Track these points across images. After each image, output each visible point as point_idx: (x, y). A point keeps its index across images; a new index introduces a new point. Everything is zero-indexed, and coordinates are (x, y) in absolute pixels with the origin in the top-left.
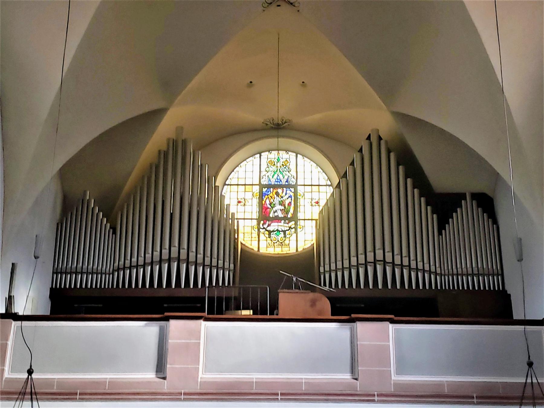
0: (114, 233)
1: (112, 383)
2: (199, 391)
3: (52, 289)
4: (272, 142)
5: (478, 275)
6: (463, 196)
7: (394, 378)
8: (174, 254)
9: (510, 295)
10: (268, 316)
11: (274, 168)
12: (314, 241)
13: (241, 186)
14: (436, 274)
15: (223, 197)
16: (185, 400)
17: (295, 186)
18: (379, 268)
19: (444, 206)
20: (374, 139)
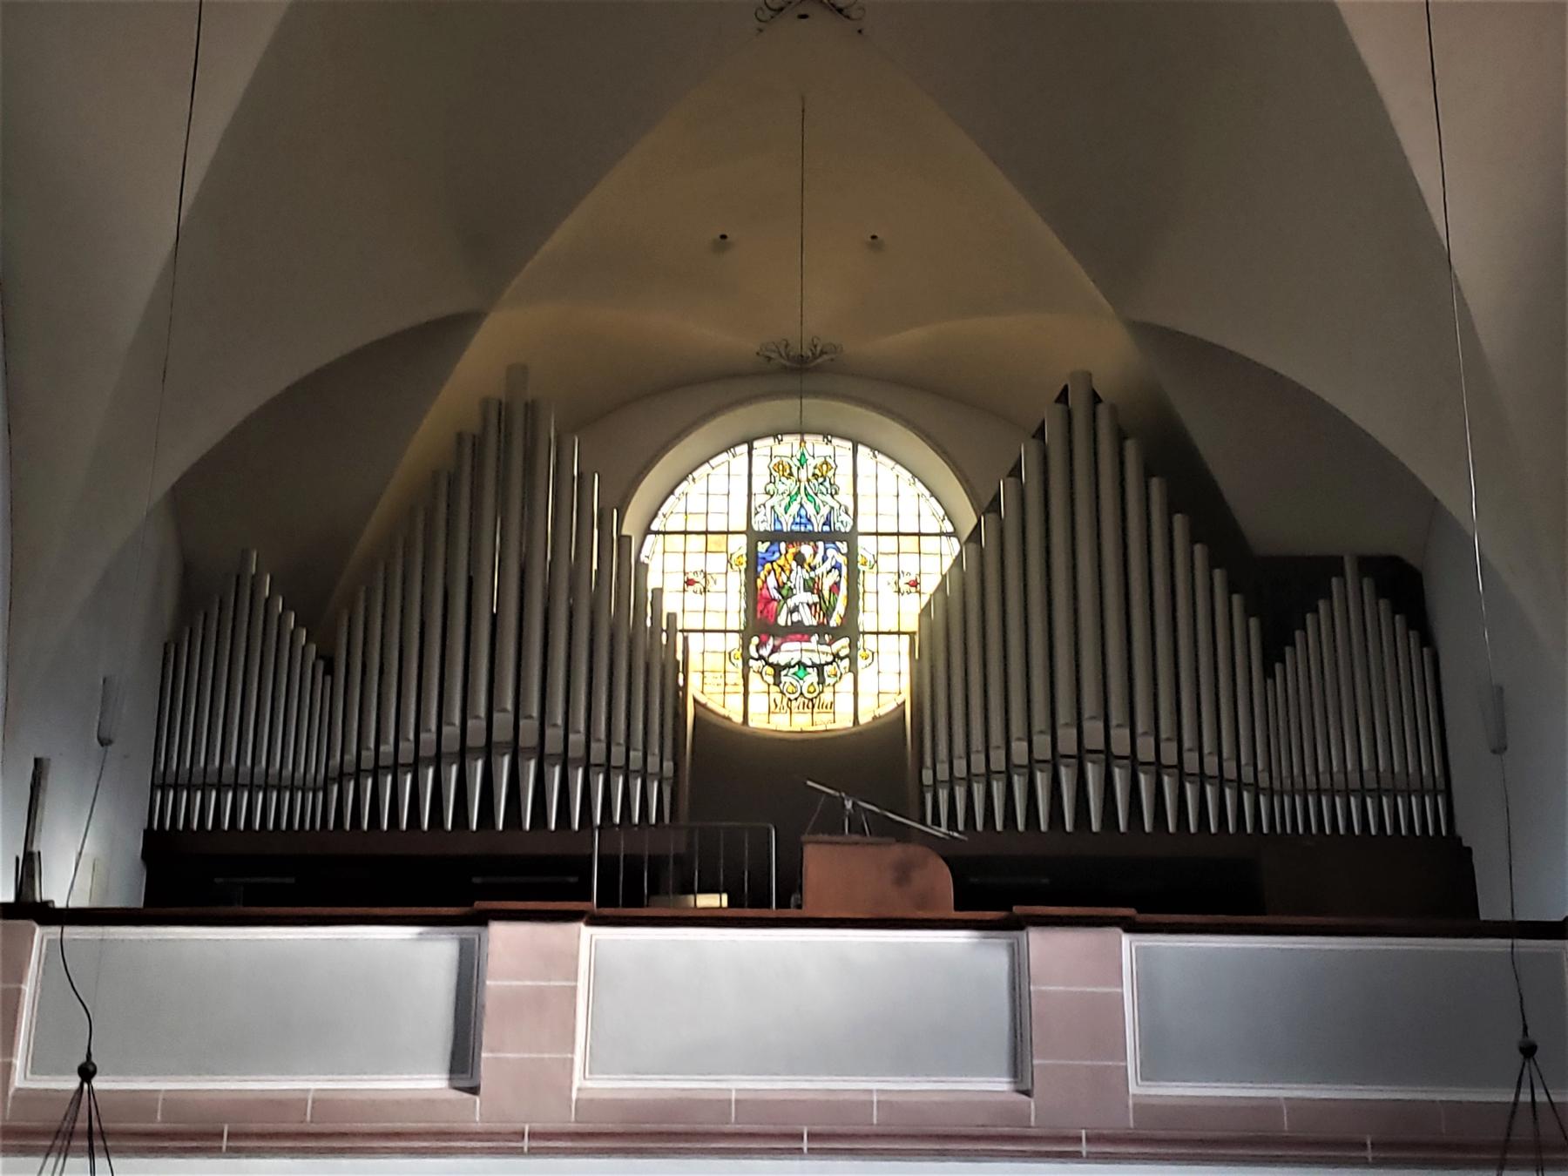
0: (330, 670)
1: (324, 1103)
2: (572, 1126)
3: (149, 834)
4: (785, 409)
5: (1378, 794)
6: (1334, 565)
7: (1136, 1088)
8: (502, 733)
9: (1469, 850)
10: (773, 912)
11: (790, 485)
12: (906, 696)
13: (695, 535)
14: (1256, 791)
15: (642, 568)
16: (533, 1152)
17: (851, 537)
18: (1092, 772)
19: (1280, 594)
20: (1078, 402)
